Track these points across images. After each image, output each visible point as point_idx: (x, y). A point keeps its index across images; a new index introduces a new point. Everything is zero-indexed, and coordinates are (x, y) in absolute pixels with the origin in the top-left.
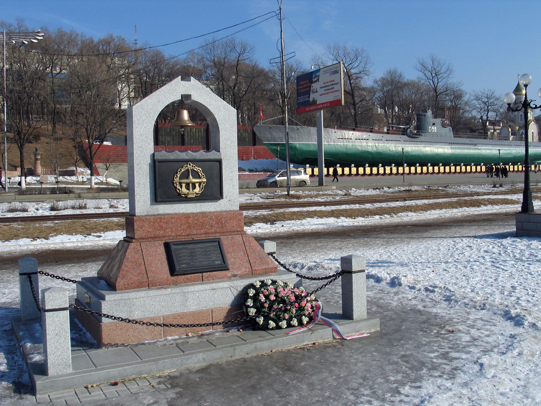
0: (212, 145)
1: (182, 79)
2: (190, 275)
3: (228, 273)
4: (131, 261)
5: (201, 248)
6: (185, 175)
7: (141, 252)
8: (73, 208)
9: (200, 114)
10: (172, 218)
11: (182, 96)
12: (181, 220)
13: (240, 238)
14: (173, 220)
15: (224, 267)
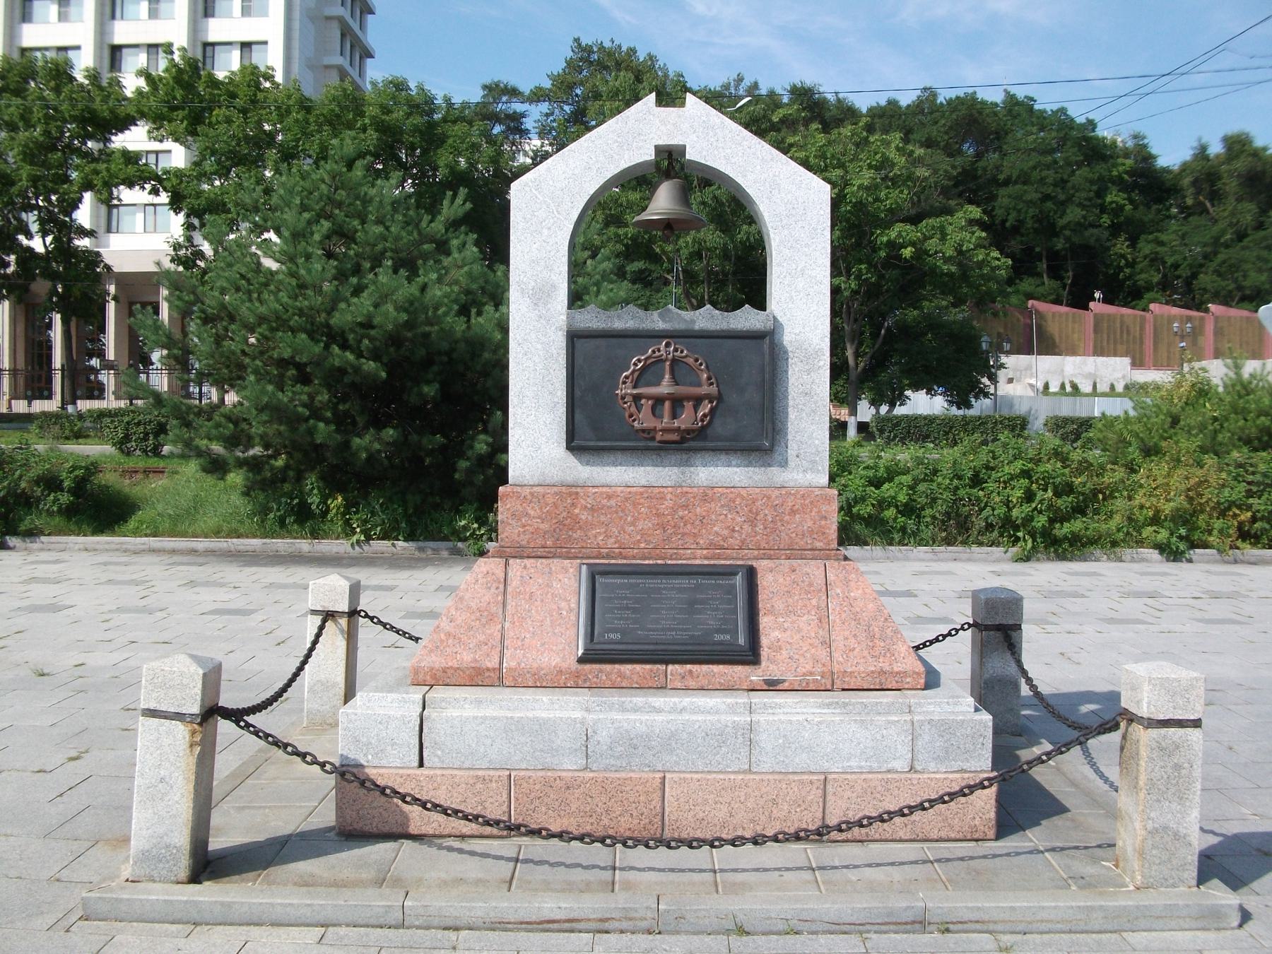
0: (209, 11)
1: (660, 102)
2: (629, 667)
3: (755, 675)
4: (469, 608)
5: (680, 590)
6: (647, 374)
7: (502, 586)
8: (706, 558)
9: (731, 210)
10: (609, 497)
11: (659, 150)
12: (635, 505)
13: (820, 573)
14: (613, 502)
15: (751, 655)
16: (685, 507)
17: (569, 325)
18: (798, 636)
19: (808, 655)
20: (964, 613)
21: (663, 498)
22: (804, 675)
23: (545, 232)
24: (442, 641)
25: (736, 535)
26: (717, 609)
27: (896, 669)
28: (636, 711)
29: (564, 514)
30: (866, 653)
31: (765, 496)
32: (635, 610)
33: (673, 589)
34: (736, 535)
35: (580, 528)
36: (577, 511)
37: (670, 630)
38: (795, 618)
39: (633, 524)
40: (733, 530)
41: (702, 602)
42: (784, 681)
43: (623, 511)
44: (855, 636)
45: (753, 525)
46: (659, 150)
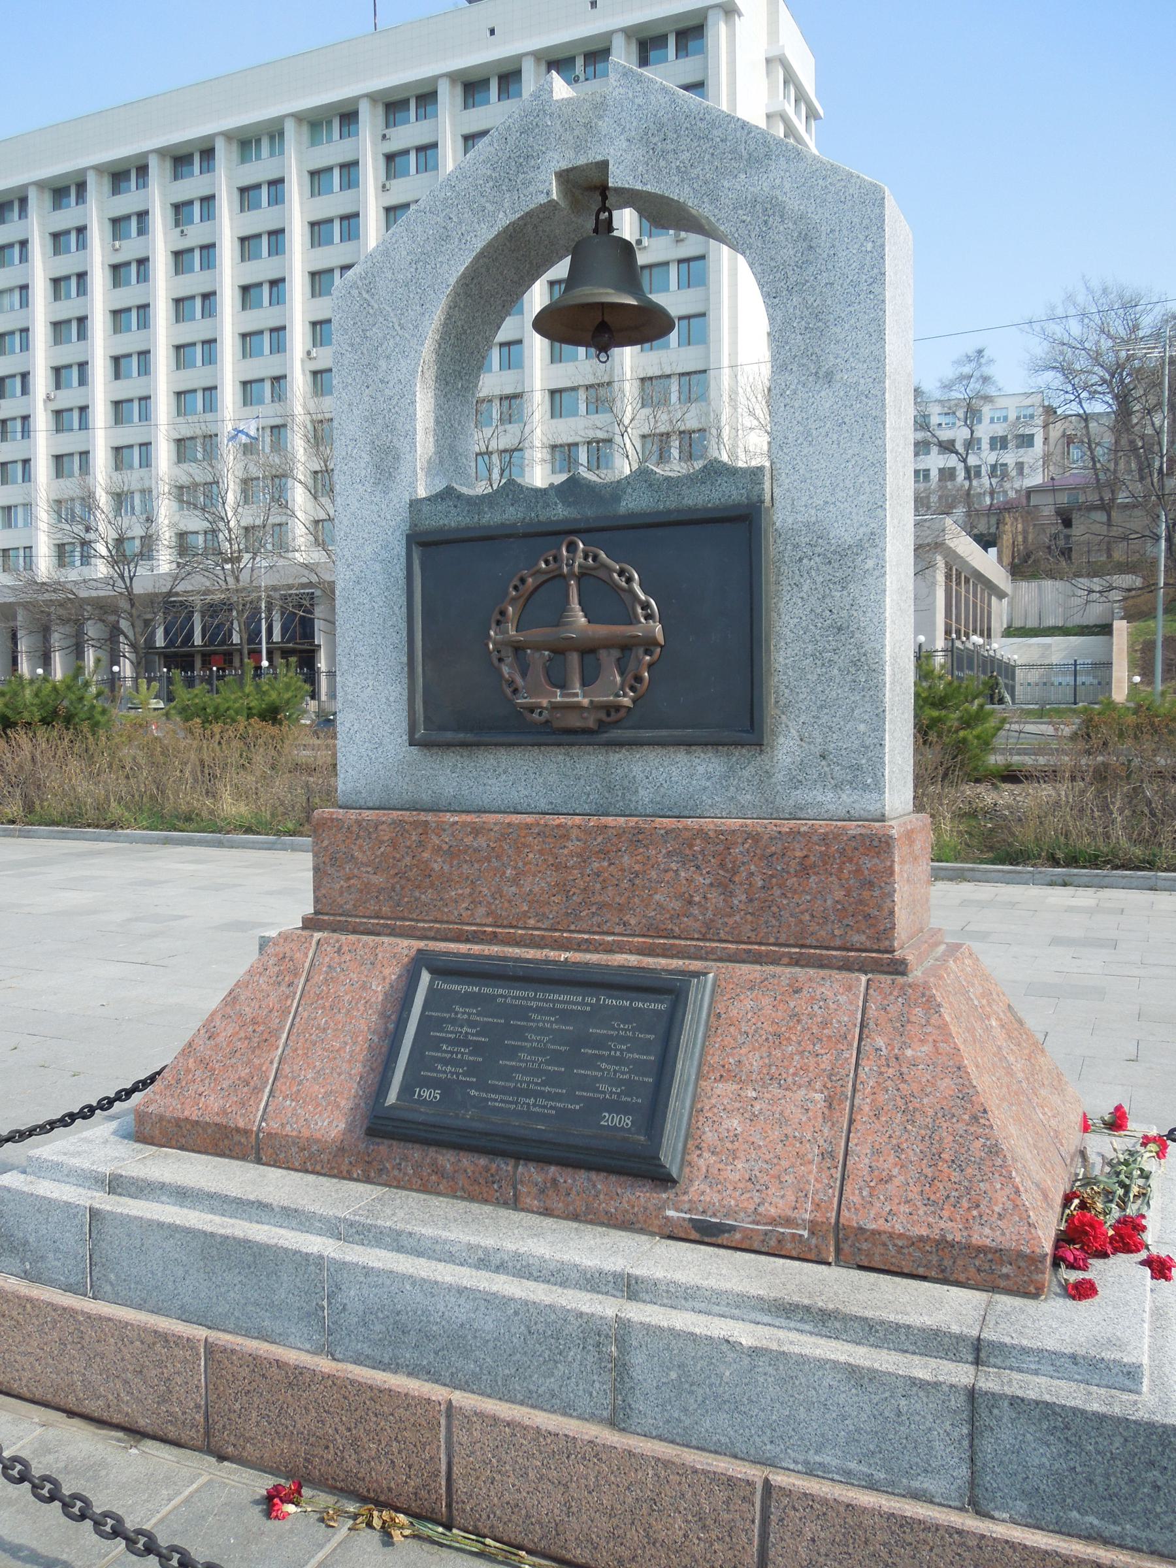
5: (565, 1016)
14: (482, 842)
16: (603, 853)
17: (413, 525)
18: (776, 1134)
19: (789, 1179)
20: (1141, 1135)
21: (566, 837)
22: (773, 1221)
23: (383, 363)
24: (188, 1071)
25: (695, 911)
26: (619, 1061)
27: (976, 1240)
28: (420, 1254)
29: (408, 860)
30: (914, 1194)
31: (749, 835)
32: (477, 1048)
33: (552, 1012)
34: (695, 911)
35: (432, 885)
36: (426, 855)
37: (528, 1093)
38: (777, 1092)
39: (515, 881)
40: (690, 903)
41: (600, 1043)
42: (732, 1229)
43: (498, 857)
44: (898, 1148)
45: (728, 894)
46: (566, 177)
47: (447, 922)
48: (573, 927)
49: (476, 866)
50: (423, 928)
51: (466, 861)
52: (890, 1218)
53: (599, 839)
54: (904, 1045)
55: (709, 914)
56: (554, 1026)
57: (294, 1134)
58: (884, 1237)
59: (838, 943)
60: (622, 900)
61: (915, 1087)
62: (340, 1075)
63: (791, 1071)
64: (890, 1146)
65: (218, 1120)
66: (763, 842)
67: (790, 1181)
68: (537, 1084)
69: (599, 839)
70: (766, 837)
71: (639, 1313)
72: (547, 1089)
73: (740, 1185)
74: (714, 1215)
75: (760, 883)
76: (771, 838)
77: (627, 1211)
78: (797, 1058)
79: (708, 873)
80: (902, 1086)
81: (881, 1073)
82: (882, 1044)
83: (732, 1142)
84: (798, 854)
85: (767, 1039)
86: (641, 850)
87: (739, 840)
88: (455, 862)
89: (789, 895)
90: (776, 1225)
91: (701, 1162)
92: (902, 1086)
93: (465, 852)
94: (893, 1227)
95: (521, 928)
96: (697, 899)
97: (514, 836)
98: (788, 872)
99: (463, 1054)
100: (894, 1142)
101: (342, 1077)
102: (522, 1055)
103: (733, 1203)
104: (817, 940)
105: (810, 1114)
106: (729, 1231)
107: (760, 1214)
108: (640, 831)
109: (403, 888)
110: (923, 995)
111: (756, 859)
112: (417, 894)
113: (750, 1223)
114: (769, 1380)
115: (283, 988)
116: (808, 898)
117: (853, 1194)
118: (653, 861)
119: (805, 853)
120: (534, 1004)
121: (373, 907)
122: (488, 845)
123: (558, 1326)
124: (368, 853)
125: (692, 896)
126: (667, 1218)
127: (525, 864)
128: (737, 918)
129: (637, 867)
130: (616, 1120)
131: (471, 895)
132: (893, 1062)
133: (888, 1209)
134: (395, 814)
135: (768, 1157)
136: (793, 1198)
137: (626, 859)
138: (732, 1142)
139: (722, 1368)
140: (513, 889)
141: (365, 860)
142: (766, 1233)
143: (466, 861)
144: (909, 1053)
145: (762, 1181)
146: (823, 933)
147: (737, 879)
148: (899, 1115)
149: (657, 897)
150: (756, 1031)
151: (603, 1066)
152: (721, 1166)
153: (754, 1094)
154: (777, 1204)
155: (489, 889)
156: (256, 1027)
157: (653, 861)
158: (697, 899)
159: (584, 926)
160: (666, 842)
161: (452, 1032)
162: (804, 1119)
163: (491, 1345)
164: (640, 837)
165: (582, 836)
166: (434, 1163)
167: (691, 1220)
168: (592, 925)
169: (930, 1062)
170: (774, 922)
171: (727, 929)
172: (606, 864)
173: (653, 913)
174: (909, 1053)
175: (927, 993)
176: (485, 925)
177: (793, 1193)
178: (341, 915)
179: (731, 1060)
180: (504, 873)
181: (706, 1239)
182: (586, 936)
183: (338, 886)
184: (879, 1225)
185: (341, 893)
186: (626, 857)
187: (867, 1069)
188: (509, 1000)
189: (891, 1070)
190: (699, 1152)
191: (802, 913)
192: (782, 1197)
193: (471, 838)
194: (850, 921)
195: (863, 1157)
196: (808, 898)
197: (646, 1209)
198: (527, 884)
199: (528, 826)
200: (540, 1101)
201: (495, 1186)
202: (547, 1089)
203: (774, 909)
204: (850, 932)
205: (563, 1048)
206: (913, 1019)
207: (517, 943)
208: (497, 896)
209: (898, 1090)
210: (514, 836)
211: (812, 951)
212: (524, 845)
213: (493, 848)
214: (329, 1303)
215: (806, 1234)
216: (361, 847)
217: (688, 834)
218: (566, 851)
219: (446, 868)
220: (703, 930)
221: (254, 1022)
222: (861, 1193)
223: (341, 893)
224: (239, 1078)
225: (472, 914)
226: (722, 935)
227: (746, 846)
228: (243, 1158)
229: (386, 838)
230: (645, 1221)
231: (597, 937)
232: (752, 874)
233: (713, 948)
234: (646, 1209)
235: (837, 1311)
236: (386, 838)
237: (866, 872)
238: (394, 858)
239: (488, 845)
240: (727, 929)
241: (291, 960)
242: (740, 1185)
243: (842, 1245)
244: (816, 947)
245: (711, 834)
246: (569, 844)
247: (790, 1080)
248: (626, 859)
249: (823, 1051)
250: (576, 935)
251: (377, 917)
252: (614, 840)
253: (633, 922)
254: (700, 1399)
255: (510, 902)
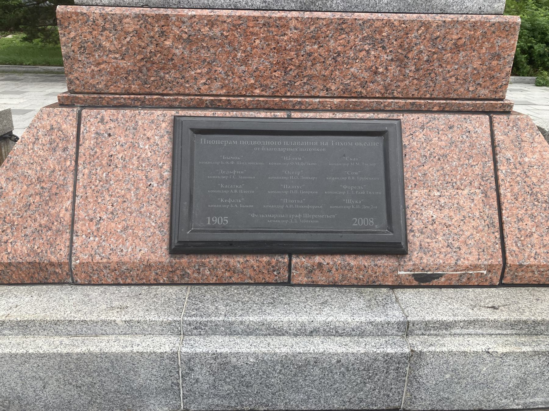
14: (217, 31)
16: (315, 38)
21: (286, 26)
22: (467, 268)
25: (379, 78)
29: (152, 48)
36: (168, 43)
39: (244, 62)
40: (376, 73)
42: (441, 276)
44: (532, 216)
47: (189, 95)
48: (289, 94)
49: (212, 50)
50: (169, 100)
51: (203, 47)
52: (536, 257)
53: (312, 28)
54: (523, 155)
55: (388, 80)
56: (302, 164)
57: (105, 260)
58: (534, 268)
59: (470, 95)
60: (327, 73)
61: (535, 180)
62: (131, 213)
63: (458, 177)
64: (527, 216)
65: (29, 259)
66: (431, 30)
67: (472, 244)
68: (300, 204)
69: (312, 28)
70: (435, 25)
71: (417, 343)
72: (308, 207)
73: (443, 250)
74: (430, 270)
75: (425, 58)
76: (438, 26)
77: (371, 276)
78: (460, 169)
79: (391, 51)
80: (526, 179)
81: (513, 173)
82: (509, 155)
83: (432, 224)
84: (455, 37)
85: (439, 159)
86: (344, 36)
87: (416, 28)
88: (194, 48)
89: (444, 65)
90: (468, 270)
91: (416, 240)
92: (526, 179)
93: (203, 40)
94: (539, 261)
95: (249, 96)
96: (381, 70)
97: (244, 26)
98: (446, 50)
99: (238, 189)
100: (529, 213)
101: (134, 215)
102: (285, 186)
103: (441, 261)
104: (458, 95)
105: (475, 202)
106: (438, 278)
107: (459, 266)
108: (344, 21)
109: (148, 70)
110: (528, 125)
111: (425, 41)
112: (162, 74)
113: (452, 271)
114: (511, 367)
115: (59, 152)
116: (456, 67)
117: (512, 246)
118: (352, 43)
119: (459, 36)
120: (283, 150)
121: (122, 85)
122: (222, 34)
123: (369, 364)
124: (115, 42)
125: (377, 68)
126: (398, 276)
127: (253, 48)
128: (407, 82)
129: (339, 49)
130: (363, 222)
131: (208, 73)
132: (518, 166)
133: (534, 252)
134: (137, 10)
135: (456, 231)
136: (477, 253)
137: (332, 43)
138: (432, 224)
139: (481, 366)
140: (243, 68)
141: (112, 48)
142: (461, 276)
143: (203, 47)
144: (527, 159)
145: (456, 246)
146: (462, 90)
147: (410, 56)
148: (529, 196)
149: (352, 70)
150: (431, 154)
151: (345, 187)
152: (429, 240)
153: (439, 194)
154: (469, 258)
155: (223, 68)
156: (43, 184)
157: (352, 43)
158: (381, 70)
159: (297, 93)
160: (362, 29)
161: (225, 175)
162: (472, 205)
163: (317, 383)
164: (344, 26)
165: (299, 25)
166: (228, 264)
167: (414, 275)
168: (304, 92)
169: (539, 164)
170: (431, 84)
171: (399, 90)
172: (316, 47)
173: (349, 82)
174: (527, 159)
175: (530, 123)
176: (220, 95)
177: (475, 249)
178: (94, 93)
179: (419, 174)
180: (236, 55)
181: (422, 284)
182: (299, 100)
183: (89, 70)
184: (532, 261)
185: (93, 77)
186: (332, 41)
187: (504, 171)
188: (263, 149)
189: (518, 171)
190: (413, 233)
191: (451, 77)
192: (470, 253)
193: (207, 29)
194: (480, 81)
195: (513, 224)
196: (456, 67)
197: (384, 273)
198: (254, 63)
199: (256, 19)
200: (306, 216)
201: (275, 273)
202: (308, 207)
203: (433, 75)
204: (479, 88)
205: (313, 178)
206: (524, 139)
207: (247, 108)
208: (230, 73)
209: (525, 182)
210: (244, 26)
211: (454, 101)
212: (252, 34)
213: (226, 37)
214: (184, 380)
215: (485, 272)
216: (107, 38)
217: (379, 24)
218: (286, 38)
219: (186, 53)
220: (383, 91)
221: (39, 180)
222: (517, 245)
223: (93, 77)
224: (40, 226)
225: (210, 88)
226: (395, 94)
227: (420, 32)
228: (61, 283)
229: (130, 30)
230: (383, 280)
231: (307, 100)
232: (422, 52)
233: (389, 103)
234: (384, 273)
235: (543, 320)
236: (130, 30)
237: (497, 48)
238: (140, 46)
239: (222, 34)
240: (399, 90)
241: (60, 129)
242: (443, 250)
243: (506, 275)
244: (456, 99)
245: (396, 23)
246: (289, 32)
247: (458, 183)
248: (332, 43)
249: (475, 164)
250: (291, 99)
251: (129, 94)
252: (324, 29)
253: (333, 88)
254: (463, 385)
255: (240, 77)
